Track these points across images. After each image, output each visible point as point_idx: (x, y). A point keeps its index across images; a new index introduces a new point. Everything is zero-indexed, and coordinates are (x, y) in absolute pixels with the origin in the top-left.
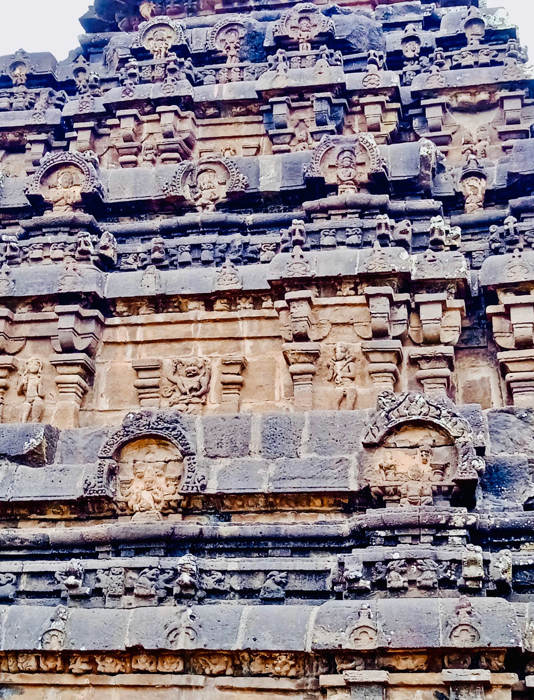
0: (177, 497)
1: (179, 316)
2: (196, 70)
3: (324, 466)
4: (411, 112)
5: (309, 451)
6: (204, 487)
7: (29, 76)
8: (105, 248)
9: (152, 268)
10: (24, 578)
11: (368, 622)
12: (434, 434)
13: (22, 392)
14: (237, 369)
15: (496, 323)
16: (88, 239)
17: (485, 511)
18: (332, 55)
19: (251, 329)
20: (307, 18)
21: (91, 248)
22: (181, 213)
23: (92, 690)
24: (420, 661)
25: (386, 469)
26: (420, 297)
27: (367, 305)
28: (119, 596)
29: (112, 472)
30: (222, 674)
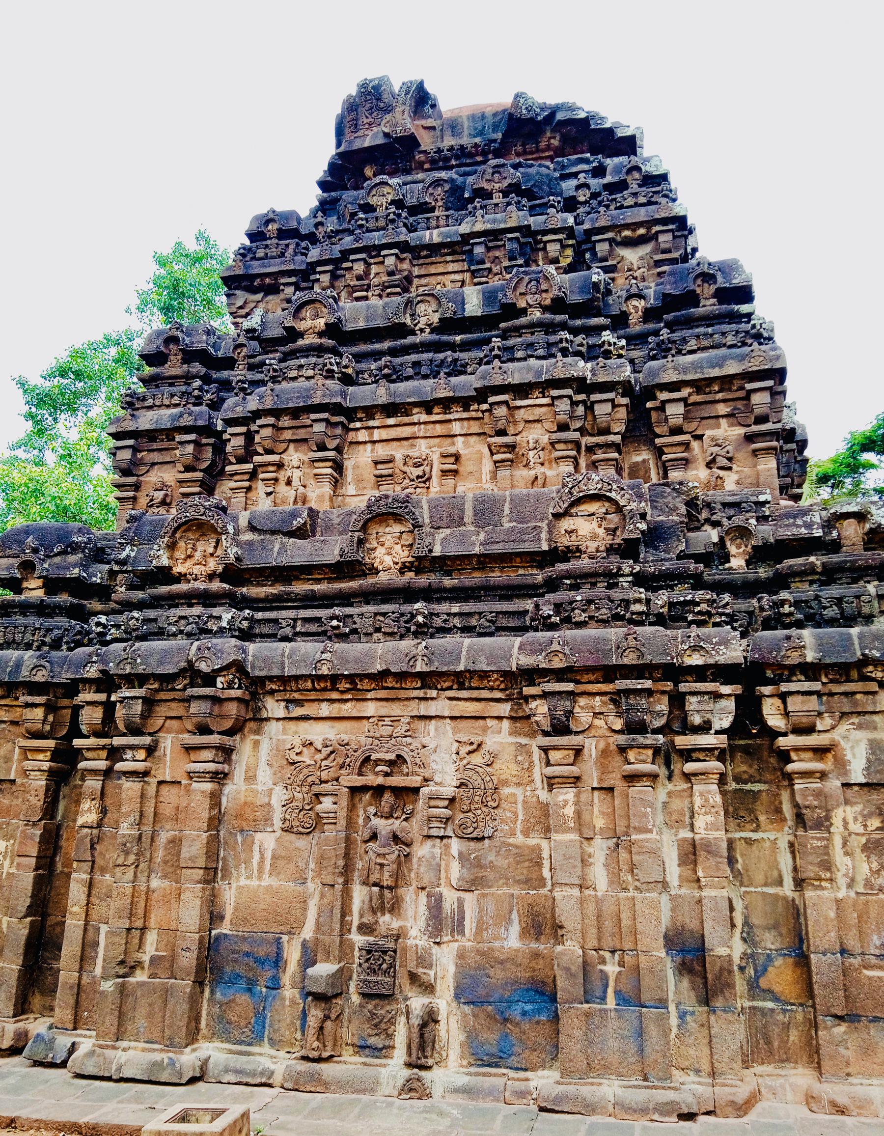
0: (410, 559)
1: (406, 419)
2: (411, 219)
3: (522, 532)
4: (584, 247)
5: (510, 521)
6: (431, 551)
8: (346, 367)
9: (383, 382)
10: (299, 623)
11: (558, 648)
12: (607, 504)
13: (289, 483)
15: (654, 415)
16: (333, 361)
17: (648, 562)
18: (519, 202)
19: (462, 428)
20: (499, 172)
21: (335, 368)
23: (354, 703)
25: (570, 532)
26: (595, 397)
27: (552, 405)
28: (371, 634)
29: (361, 542)
30: (450, 688)
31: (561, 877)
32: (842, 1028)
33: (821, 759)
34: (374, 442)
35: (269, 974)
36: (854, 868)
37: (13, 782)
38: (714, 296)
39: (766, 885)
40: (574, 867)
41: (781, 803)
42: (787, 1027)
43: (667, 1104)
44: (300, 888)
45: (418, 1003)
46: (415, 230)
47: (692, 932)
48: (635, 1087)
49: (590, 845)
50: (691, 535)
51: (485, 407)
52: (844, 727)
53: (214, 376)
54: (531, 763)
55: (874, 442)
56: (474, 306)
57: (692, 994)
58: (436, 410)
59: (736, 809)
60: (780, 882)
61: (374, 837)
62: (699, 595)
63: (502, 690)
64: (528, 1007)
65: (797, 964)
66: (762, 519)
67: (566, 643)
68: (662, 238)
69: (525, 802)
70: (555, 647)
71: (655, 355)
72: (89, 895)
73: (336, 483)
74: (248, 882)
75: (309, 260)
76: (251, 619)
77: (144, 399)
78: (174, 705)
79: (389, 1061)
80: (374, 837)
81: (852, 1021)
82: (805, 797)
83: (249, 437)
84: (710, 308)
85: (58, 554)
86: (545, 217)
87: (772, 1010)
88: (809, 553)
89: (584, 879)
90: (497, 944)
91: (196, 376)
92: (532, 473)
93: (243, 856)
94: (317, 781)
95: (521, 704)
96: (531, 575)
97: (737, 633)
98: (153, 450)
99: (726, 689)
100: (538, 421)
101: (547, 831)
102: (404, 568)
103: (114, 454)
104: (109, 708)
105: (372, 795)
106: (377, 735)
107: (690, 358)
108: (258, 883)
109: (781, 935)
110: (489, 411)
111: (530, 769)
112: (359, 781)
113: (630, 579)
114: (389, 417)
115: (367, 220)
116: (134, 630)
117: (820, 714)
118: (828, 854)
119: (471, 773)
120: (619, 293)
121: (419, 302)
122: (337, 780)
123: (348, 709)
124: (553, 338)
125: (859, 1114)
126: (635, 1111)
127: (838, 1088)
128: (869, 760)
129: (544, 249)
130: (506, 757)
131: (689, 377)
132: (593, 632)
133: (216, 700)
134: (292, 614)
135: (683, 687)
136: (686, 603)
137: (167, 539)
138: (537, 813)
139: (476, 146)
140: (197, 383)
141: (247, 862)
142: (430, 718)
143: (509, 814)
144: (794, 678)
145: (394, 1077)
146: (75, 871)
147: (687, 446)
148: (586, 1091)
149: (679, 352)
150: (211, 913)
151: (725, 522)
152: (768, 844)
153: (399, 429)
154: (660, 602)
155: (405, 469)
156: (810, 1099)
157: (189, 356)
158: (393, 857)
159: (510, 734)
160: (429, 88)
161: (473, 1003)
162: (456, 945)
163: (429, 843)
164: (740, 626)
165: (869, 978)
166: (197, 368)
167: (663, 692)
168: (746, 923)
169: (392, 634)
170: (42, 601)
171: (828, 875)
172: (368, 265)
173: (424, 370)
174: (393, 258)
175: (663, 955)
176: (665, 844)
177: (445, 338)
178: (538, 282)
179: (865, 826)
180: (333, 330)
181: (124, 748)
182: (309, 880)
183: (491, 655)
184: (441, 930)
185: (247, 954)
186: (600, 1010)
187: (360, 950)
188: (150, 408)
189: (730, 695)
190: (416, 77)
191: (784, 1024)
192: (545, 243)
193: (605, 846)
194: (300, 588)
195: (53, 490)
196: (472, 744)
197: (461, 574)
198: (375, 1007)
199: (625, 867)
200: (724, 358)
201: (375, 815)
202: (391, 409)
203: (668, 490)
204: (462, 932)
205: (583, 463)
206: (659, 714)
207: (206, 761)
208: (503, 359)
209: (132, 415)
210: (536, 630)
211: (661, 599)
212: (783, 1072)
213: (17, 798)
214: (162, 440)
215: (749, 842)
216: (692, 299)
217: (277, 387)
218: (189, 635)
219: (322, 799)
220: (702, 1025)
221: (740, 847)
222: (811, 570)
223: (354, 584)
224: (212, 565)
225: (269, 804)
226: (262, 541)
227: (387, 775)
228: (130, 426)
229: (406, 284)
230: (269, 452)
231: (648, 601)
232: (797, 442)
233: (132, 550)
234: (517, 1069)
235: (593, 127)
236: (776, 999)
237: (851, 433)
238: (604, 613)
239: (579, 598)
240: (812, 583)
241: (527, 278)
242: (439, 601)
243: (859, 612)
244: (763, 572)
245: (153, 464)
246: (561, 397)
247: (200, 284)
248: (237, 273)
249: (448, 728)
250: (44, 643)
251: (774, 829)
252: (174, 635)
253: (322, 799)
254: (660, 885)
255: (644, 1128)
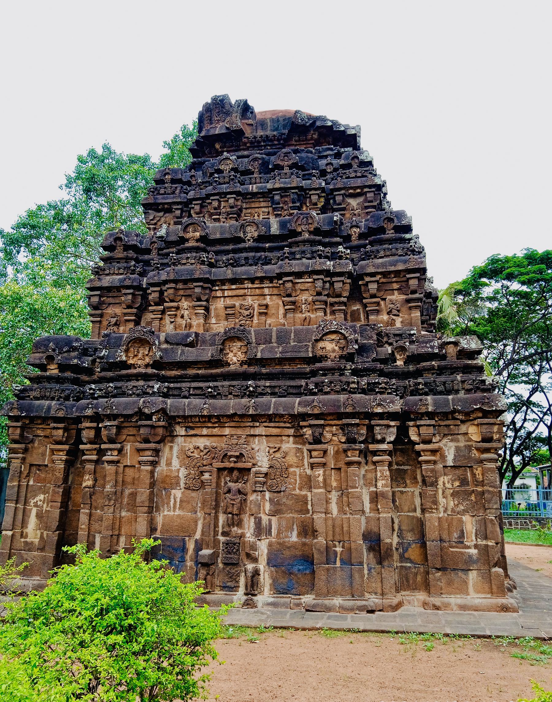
0: (245, 359)
1: (242, 286)
2: (242, 178)
3: (300, 347)
4: (330, 197)
5: (294, 342)
6: (256, 356)
7: (172, 179)
8: (211, 259)
9: (229, 267)
10: (192, 390)
11: (317, 404)
12: (340, 335)
13: (182, 317)
14: (264, 307)
15: (363, 288)
16: (204, 256)
17: (358, 363)
18: (297, 173)
19: (269, 292)
20: (287, 156)
21: (205, 259)
22: (240, 243)
24: (335, 417)
25: (322, 348)
26: (335, 279)
27: (314, 282)
29: (222, 350)
30: (265, 422)
31: (317, 508)
32: (439, 574)
33: (434, 455)
34: (225, 297)
35: (180, 555)
36: (447, 504)
37: (46, 466)
38: (393, 229)
39: (409, 512)
40: (323, 504)
41: (417, 475)
42: (416, 574)
43: (362, 606)
44: (194, 516)
45: (250, 567)
46: (244, 184)
47: (375, 533)
48: (348, 600)
49: (330, 494)
50: (379, 349)
51: (281, 282)
52: (445, 440)
53: (140, 258)
54: (303, 457)
55: (485, 273)
56: (275, 229)
57: (374, 560)
58: (256, 282)
59: (396, 478)
60: (415, 510)
61: (229, 491)
62: (382, 379)
63: (290, 423)
64: (301, 567)
65: (421, 547)
66: (412, 342)
67: (320, 402)
68: (368, 195)
69: (300, 475)
70: (315, 404)
71: (364, 258)
72: (90, 520)
73: (207, 317)
74: (169, 513)
75: (188, 198)
76: (168, 388)
77: (104, 270)
78: (131, 429)
79: (237, 593)
80: (229, 491)
81: (444, 571)
82: (427, 472)
83: (161, 293)
84: (391, 235)
85: (66, 352)
86: (310, 181)
87: (410, 567)
88: (432, 360)
89: (327, 509)
90: (287, 540)
91: (132, 259)
92: (304, 315)
93: (165, 501)
94: (202, 465)
95: (298, 430)
96: (304, 368)
97: (398, 397)
98: (110, 297)
99: (392, 423)
100: (307, 290)
101: (310, 488)
102: (242, 363)
103: (89, 298)
104: (98, 430)
105: (228, 472)
106: (230, 444)
107: (380, 260)
108: (173, 513)
109: (414, 533)
110: (283, 284)
111: (302, 460)
112: (221, 465)
113: (350, 371)
114: (233, 284)
115: (219, 178)
116: (110, 392)
117: (434, 435)
118: (436, 498)
119: (275, 462)
120: (347, 224)
121: (247, 225)
122: (211, 464)
123: (216, 431)
124: (314, 249)
125: (445, 610)
126: (348, 610)
127: (436, 599)
128: (455, 455)
129: (310, 197)
130: (292, 454)
131: (380, 270)
132: (333, 397)
133: (152, 427)
134: (188, 385)
135: (373, 422)
136: (375, 383)
137: (124, 347)
138: (306, 480)
139: (274, 136)
140: (133, 263)
141: (168, 504)
142: (256, 436)
143: (292, 480)
144: (423, 419)
145: (240, 599)
146: (82, 509)
147: (378, 304)
148: (327, 602)
149: (375, 257)
150: (151, 527)
151: (394, 343)
152: (410, 493)
153: (237, 291)
154: (363, 383)
155: (241, 311)
156: (425, 605)
157: (127, 248)
158: (238, 500)
159: (293, 443)
160: (250, 103)
161: (276, 566)
162: (268, 540)
163: (255, 494)
164: (400, 393)
165: (452, 552)
166: (131, 254)
167: (364, 425)
168: (399, 529)
169: (237, 396)
170: (59, 376)
171: (435, 507)
172: (220, 202)
173: (250, 261)
174: (233, 199)
175: (362, 543)
176: (364, 494)
177: (261, 245)
178: (307, 219)
179: (453, 485)
180: (203, 239)
181: (107, 450)
182: (198, 512)
183: (285, 407)
184: (261, 534)
185: (169, 546)
186: (333, 567)
187: (223, 543)
188: (107, 275)
189: (394, 426)
190: (242, 97)
191: (415, 573)
192: (311, 195)
193: (336, 495)
194: (192, 372)
195: (28, 300)
196: (275, 448)
197: (271, 367)
198: (230, 569)
199: (345, 504)
200: (397, 261)
201: (229, 481)
202: (233, 281)
203: (369, 328)
204: (270, 534)
205: (328, 311)
206: (362, 435)
207: (147, 457)
208: (290, 258)
209: (99, 279)
210: (306, 395)
211: (364, 381)
212: (414, 594)
213: (49, 474)
214: (114, 292)
215: (402, 492)
216: (382, 230)
217: (176, 268)
218: (138, 395)
219: (204, 474)
220: (378, 573)
221: (398, 495)
222: (432, 368)
223: (218, 371)
224: (147, 360)
225: (178, 476)
226: (172, 348)
227: (235, 462)
228: (98, 284)
229: (239, 214)
230: (172, 301)
231: (358, 382)
232: (433, 298)
233: (106, 352)
234: (296, 595)
235: (335, 129)
236: (411, 562)
237: (474, 267)
238: (338, 388)
239: (326, 381)
240: (433, 374)
241: (302, 217)
242: (259, 380)
243: (453, 388)
244: (411, 368)
245: (110, 304)
246: (318, 279)
247: (108, 178)
248: (150, 202)
249: (264, 440)
250: (61, 397)
251: (413, 487)
252: (131, 395)
253: (204, 474)
254: (361, 512)
255: (352, 617)
